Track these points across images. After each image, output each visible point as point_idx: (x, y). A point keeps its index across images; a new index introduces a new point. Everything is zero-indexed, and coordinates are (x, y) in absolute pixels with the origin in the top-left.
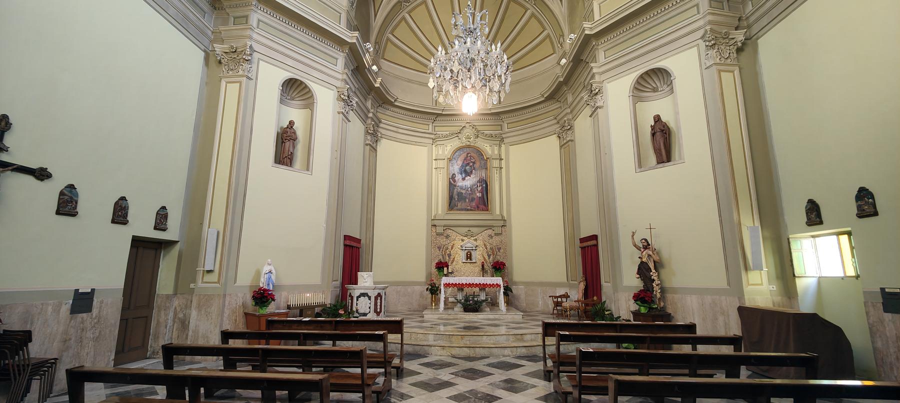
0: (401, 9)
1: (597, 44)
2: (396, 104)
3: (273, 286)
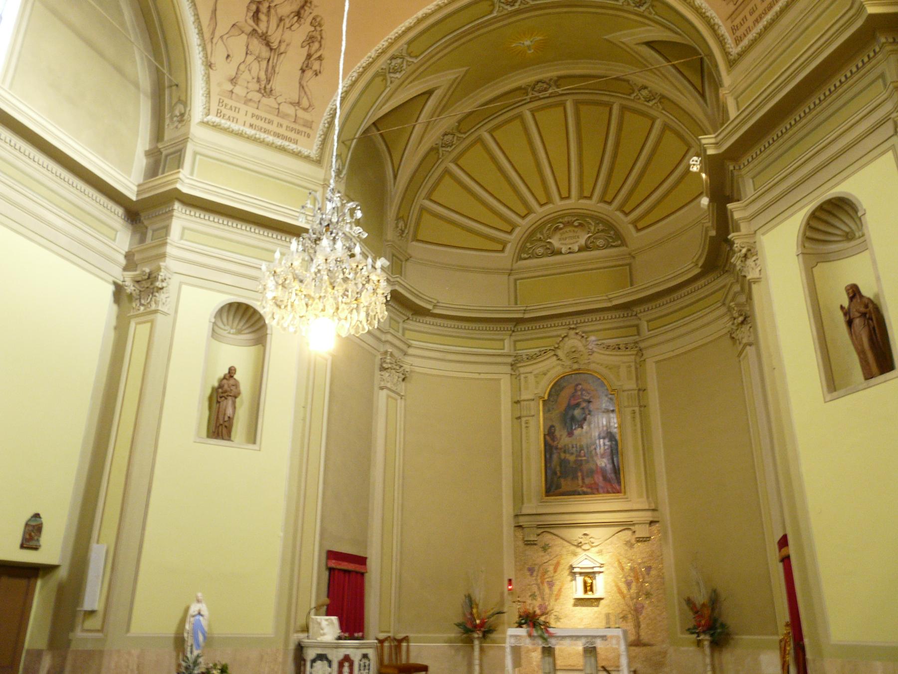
0: (438, 159)
1: (737, 168)
2: (436, 311)
3: (205, 638)
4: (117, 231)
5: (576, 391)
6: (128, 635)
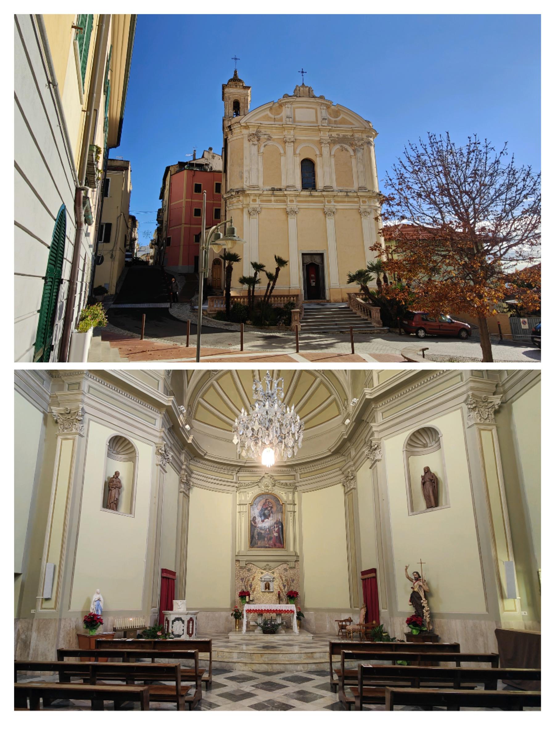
4: (44, 380)
5: (266, 502)
6: (69, 611)
